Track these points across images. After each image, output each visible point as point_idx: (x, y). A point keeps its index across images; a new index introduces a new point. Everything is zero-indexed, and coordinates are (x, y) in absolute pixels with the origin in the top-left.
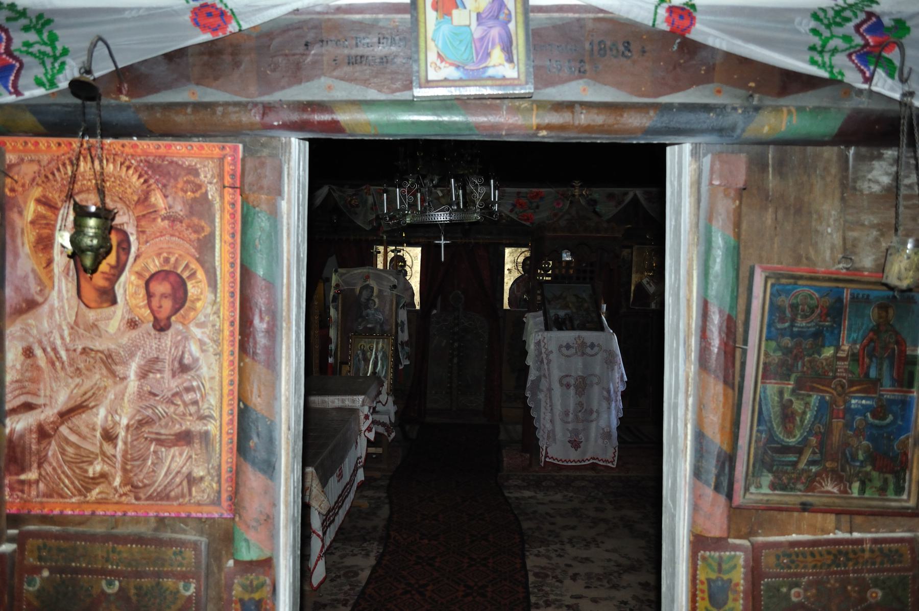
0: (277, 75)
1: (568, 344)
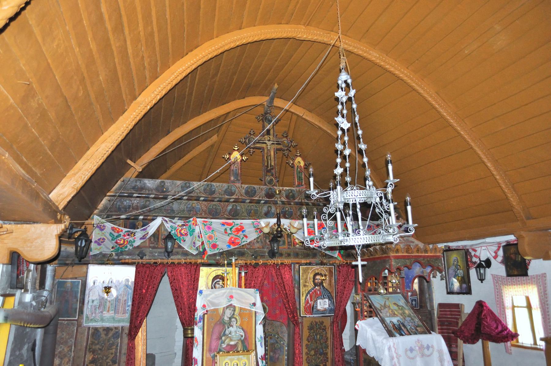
0: (387, 190)
1: (411, 348)
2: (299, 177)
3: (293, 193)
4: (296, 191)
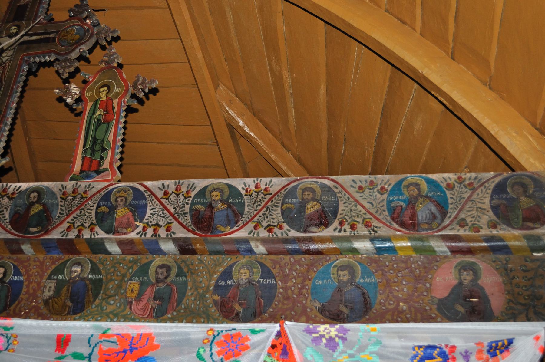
2: (95, 139)
3: (44, 205)
4: (59, 195)
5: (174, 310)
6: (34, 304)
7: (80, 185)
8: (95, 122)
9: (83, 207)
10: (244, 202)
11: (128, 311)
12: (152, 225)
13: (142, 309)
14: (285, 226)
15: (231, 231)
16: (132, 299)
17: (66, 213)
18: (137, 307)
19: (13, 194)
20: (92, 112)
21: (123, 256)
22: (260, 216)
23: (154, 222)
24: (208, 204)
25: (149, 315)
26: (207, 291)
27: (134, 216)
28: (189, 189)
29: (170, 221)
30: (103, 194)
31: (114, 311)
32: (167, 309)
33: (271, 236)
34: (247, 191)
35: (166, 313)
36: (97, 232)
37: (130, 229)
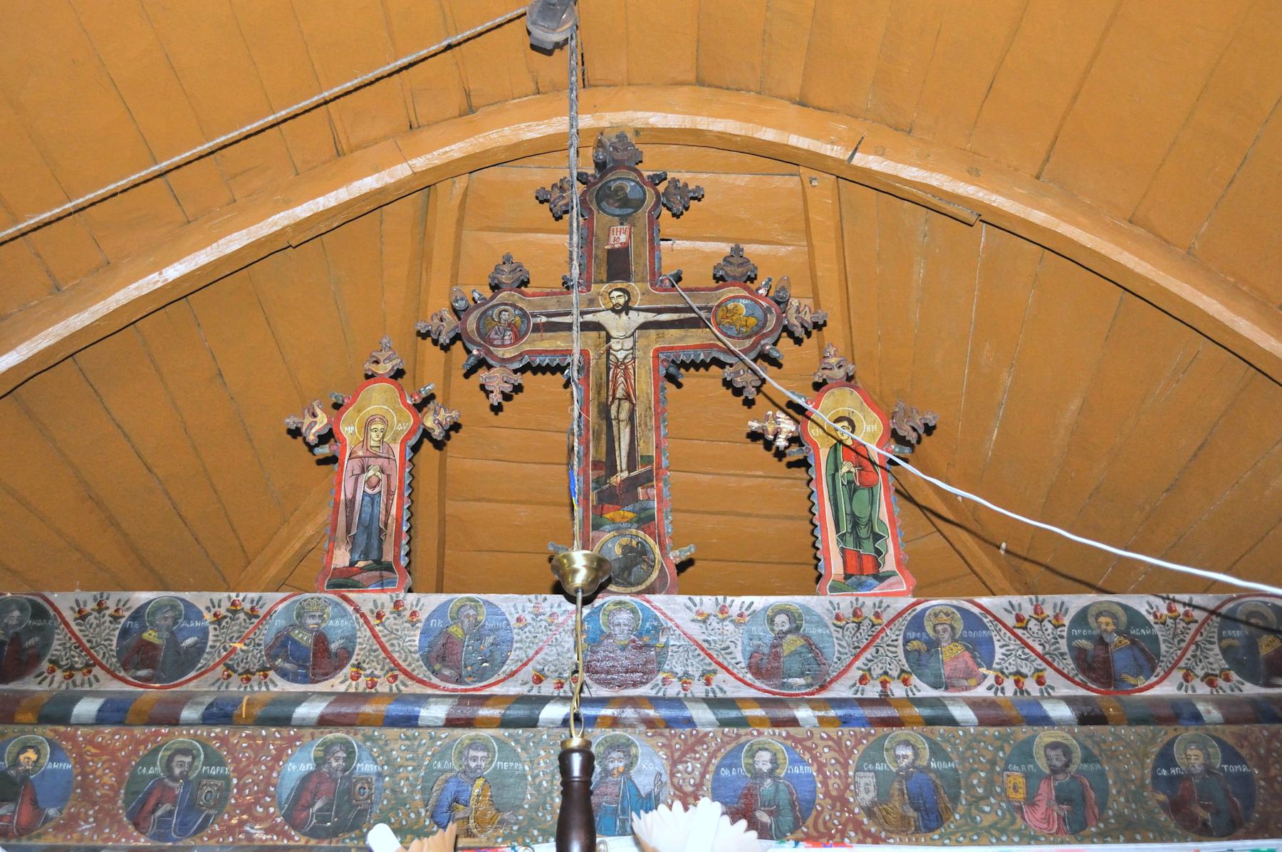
3: (807, 638)
4: (829, 620)
5: (1099, 820)
6: (847, 814)
7: (864, 603)
8: (843, 485)
9: (878, 641)
10: (1157, 636)
11: (1019, 823)
12: (1010, 674)
13: (1045, 819)
14: (1234, 676)
15: (1147, 683)
16: (1020, 802)
17: (851, 652)
18: (1034, 818)
19: (741, 615)
20: (832, 466)
21: (981, 729)
22: (1189, 659)
23: (1012, 669)
24: (1098, 638)
25: (1059, 828)
26: (1143, 787)
27: (974, 657)
28: (1058, 611)
29: (1039, 667)
30: (909, 618)
31: (996, 823)
32: (1085, 819)
33: (394, 689)
34: (1155, 616)
35: (1086, 825)
36: (915, 686)
37: (973, 682)
